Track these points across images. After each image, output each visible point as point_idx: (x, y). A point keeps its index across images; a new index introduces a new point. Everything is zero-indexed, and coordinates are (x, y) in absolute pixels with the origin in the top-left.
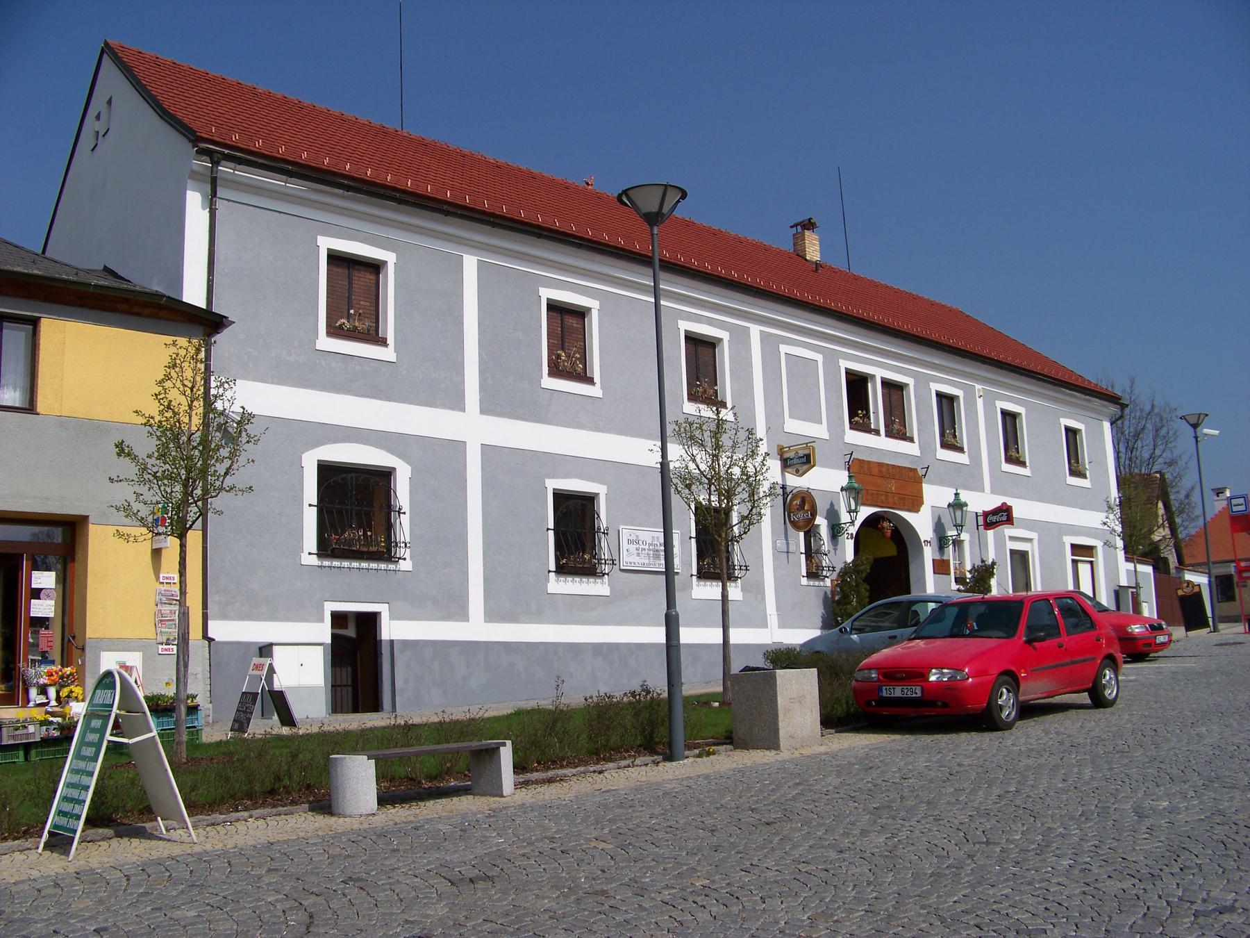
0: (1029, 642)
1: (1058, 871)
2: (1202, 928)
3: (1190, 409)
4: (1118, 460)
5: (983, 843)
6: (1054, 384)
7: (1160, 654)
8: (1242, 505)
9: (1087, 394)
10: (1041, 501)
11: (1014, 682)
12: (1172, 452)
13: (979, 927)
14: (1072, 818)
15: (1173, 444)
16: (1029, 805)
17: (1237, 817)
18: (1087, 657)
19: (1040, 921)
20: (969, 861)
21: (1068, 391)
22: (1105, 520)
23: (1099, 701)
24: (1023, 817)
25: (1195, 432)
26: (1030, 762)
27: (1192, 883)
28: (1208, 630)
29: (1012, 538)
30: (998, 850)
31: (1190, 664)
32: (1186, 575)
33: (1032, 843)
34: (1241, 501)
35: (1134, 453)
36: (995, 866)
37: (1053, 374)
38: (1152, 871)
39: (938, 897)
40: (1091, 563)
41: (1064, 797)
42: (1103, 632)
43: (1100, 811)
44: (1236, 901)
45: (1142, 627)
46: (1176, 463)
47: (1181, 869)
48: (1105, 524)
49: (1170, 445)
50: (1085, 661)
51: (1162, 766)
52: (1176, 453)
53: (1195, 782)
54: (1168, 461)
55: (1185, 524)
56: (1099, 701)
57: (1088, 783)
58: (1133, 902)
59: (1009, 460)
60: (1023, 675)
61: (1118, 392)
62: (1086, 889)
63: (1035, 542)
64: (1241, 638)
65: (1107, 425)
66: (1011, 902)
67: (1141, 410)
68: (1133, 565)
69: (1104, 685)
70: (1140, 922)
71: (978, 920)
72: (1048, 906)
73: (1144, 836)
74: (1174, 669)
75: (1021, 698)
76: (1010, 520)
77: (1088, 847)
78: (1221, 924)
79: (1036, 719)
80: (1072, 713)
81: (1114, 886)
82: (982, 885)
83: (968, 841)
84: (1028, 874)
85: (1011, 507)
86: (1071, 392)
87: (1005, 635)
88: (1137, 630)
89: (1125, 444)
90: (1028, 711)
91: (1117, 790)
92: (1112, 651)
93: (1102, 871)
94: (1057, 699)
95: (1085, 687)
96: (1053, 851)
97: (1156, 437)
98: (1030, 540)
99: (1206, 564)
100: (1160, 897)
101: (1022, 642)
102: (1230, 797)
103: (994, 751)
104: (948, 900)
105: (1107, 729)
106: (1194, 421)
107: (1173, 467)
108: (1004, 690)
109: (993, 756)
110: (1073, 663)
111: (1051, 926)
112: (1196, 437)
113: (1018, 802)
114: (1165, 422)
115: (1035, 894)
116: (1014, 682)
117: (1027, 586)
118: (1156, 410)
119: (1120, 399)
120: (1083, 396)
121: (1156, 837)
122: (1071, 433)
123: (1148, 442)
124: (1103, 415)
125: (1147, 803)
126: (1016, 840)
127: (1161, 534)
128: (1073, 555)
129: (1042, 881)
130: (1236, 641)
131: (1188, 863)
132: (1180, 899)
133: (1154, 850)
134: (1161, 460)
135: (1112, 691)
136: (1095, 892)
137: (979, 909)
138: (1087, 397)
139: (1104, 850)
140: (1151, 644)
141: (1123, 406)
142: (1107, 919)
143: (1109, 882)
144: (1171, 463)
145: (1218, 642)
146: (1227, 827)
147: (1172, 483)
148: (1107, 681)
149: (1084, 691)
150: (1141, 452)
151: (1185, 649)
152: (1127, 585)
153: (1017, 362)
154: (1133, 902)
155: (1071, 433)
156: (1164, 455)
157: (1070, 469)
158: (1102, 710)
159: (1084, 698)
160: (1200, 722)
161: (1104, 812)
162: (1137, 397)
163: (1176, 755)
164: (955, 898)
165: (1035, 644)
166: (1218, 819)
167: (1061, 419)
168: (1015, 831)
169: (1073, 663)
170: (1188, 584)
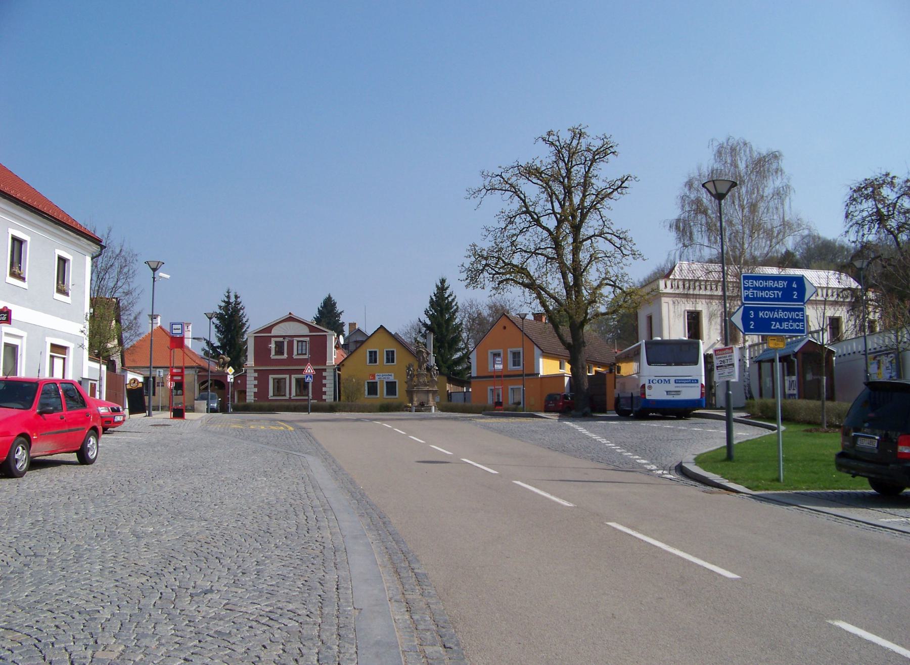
0: (41, 413)
1: (94, 573)
2: (197, 603)
3: (154, 258)
4: (652, 282)
5: (32, 556)
6: (56, 224)
7: (115, 429)
8: (179, 329)
9: (78, 234)
10: (33, 308)
11: (28, 445)
12: (129, 285)
13: (51, 611)
14: (92, 538)
15: (131, 280)
16: (57, 530)
17: (199, 537)
18: (79, 427)
19: (92, 605)
20: (26, 568)
21: (64, 229)
22: (83, 329)
23: (84, 459)
24: (56, 538)
25: (154, 274)
26: (46, 500)
27: (184, 577)
28: (144, 414)
29: (7, 334)
30: (45, 560)
31: (137, 437)
32: (128, 374)
33: (69, 555)
34: (179, 327)
35: (102, 282)
36: (47, 571)
37: (55, 215)
38: (156, 571)
39: (12, 593)
40: (64, 359)
41: (81, 525)
42: (91, 410)
43: (109, 534)
44: (212, 586)
45: (106, 409)
46: (131, 293)
47: (175, 569)
48: (82, 332)
49: (129, 280)
50: (78, 430)
51: (141, 505)
52: (133, 286)
53: (166, 515)
54: (125, 291)
55: (132, 337)
56: (84, 459)
57: (94, 516)
58: (150, 591)
59: (13, 274)
60: (34, 437)
61: (98, 235)
62: (117, 583)
63: (25, 339)
64: (168, 422)
65: (88, 259)
66: (68, 594)
67: (113, 252)
68: (99, 365)
69: (89, 448)
70: (159, 602)
71: (49, 607)
72: (95, 595)
73: (144, 550)
74: (127, 440)
75: (31, 455)
76: (8, 320)
77: (109, 557)
78: (207, 600)
79: (38, 470)
80: (63, 467)
81: (135, 581)
82: (42, 584)
83: (20, 554)
84: (73, 575)
85: (11, 311)
86: (66, 231)
87: (22, 407)
88: (102, 411)
89: (99, 275)
90: (35, 464)
91: (116, 520)
92: (95, 424)
93: (124, 572)
94: (55, 457)
95: (75, 449)
96: (85, 560)
97: (120, 272)
98: (21, 337)
99: (149, 368)
100: (166, 586)
101: (35, 413)
102: (191, 525)
103: (16, 493)
104: (21, 595)
105: (95, 479)
106: (154, 266)
107: (128, 296)
108: (20, 448)
109: (16, 495)
110: (69, 431)
111: (102, 608)
112: (154, 278)
113: (48, 527)
114: (128, 262)
115: (83, 588)
116: (28, 445)
117: (15, 371)
118: (123, 254)
119: (101, 242)
120: (75, 235)
121: (152, 550)
122: (62, 261)
123: (113, 275)
124: (88, 252)
125: (138, 529)
126: (56, 553)
127: (112, 344)
128: (51, 351)
129: (85, 579)
130: (165, 423)
131: (177, 566)
132: (179, 587)
133: (153, 558)
134: (121, 290)
135: (94, 453)
136: (123, 585)
137: (48, 599)
138: (78, 236)
139: (120, 559)
140: (110, 421)
141: (103, 247)
142: (137, 601)
143: (131, 579)
144: (127, 294)
145: (153, 424)
146: (194, 543)
147: (126, 307)
148: (91, 446)
149: (74, 452)
150: (107, 282)
151: (130, 427)
152: (87, 377)
153: (30, 202)
154: (150, 591)
155: (62, 261)
156: (123, 287)
157: (57, 288)
158: (85, 466)
159: (74, 457)
160: (158, 477)
161: (112, 535)
162: (112, 241)
163: (149, 498)
164: (26, 594)
165: (44, 415)
166: (188, 538)
167: (56, 250)
168: (53, 547)
169: (69, 431)
170: (135, 381)
